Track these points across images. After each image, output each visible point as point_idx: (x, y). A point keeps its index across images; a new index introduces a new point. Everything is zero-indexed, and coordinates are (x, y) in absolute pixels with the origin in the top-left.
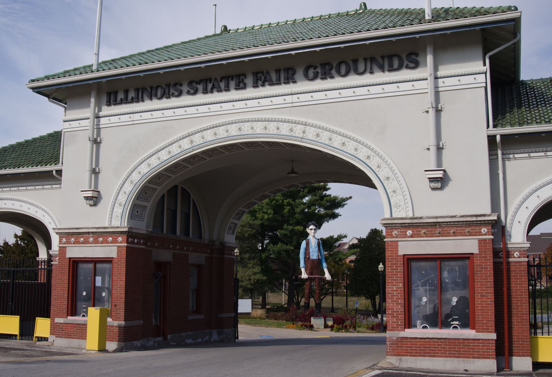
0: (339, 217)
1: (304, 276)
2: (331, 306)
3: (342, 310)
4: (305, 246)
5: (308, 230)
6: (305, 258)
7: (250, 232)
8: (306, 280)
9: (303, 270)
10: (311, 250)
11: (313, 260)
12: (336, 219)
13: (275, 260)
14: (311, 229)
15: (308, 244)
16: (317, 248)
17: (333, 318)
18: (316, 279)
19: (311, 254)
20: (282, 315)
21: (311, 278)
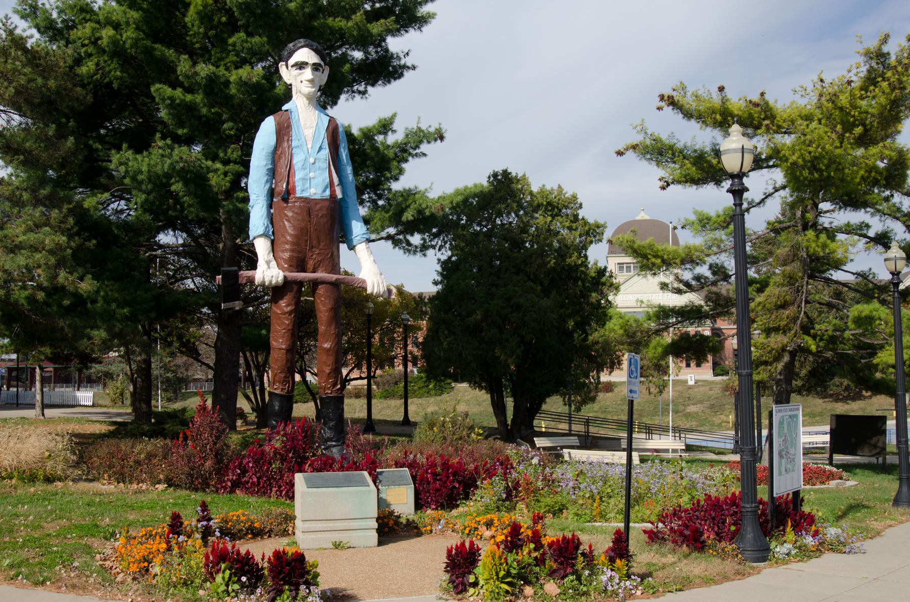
0: (407, 74)
1: (268, 271)
2: (409, 401)
3: (431, 426)
4: (273, 141)
5: (287, 74)
6: (271, 193)
7: (23, 80)
8: (278, 291)
9: (262, 247)
10: (297, 160)
11: (306, 200)
12: (395, 84)
13: (178, 254)
14: (301, 66)
15: (283, 132)
16: (326, 152)
17: (412, 466)
18: (321, 290)
19: (298, 175)
20: (150, 456)
21: (300, 283)
